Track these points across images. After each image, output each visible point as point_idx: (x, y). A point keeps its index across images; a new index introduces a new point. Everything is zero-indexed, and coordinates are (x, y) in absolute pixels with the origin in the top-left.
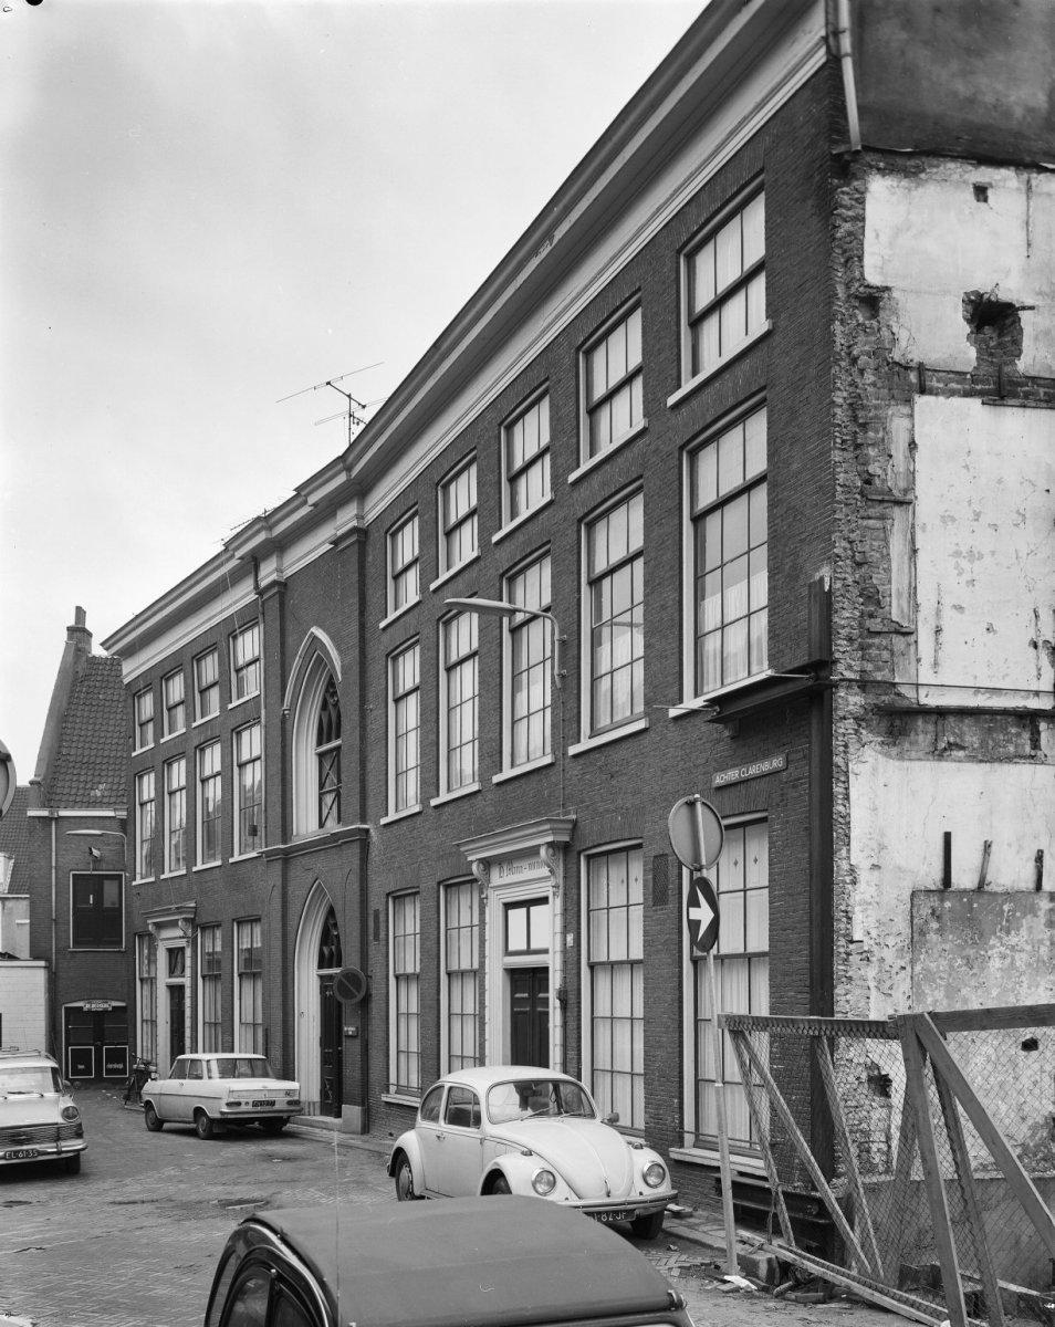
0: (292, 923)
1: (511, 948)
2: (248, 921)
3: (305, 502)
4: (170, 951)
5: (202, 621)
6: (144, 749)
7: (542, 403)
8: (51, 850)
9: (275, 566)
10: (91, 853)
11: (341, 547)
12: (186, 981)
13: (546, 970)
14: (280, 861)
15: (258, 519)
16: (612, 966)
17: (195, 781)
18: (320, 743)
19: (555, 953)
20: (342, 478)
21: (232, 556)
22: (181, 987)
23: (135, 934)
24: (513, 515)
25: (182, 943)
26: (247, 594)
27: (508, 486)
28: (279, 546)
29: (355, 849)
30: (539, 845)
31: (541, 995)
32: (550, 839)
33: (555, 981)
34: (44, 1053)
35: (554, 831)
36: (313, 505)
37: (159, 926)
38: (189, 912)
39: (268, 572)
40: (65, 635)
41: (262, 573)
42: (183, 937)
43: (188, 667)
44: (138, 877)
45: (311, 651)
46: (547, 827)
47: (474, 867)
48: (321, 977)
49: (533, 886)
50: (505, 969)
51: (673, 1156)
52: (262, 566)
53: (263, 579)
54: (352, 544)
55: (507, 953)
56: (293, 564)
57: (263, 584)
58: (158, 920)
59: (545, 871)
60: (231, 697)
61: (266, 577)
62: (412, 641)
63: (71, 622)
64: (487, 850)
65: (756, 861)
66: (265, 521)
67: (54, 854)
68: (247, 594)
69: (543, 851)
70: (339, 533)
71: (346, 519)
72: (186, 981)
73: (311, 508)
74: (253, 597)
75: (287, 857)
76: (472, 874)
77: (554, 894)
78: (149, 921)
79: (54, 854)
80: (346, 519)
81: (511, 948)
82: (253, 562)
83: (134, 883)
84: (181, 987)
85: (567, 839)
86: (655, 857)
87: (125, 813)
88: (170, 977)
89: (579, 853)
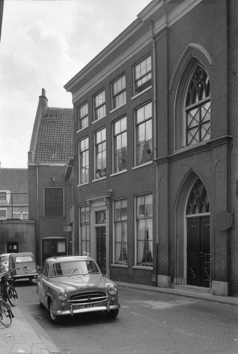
2: (119, 200)
4: (97, 213)
5: (113, 66)
7: (123, 78)
8: (36, 179)
9: (165, 21)
10: (52, 179)
12: (107, 225)
13: (105, 227)
17: (93, 148)
19: (107, 223)
22: (103, 229)
24: (114, 107)
25: (105, 208)
27: (113, 99)
30: (104, 198)
31: (104, 234)
32: (107, 196)
33: (107, 230)
34: (87, 264)
35: (107, 194)
40: (38, 99)
41: (156, 27)
42: (106, 205)
46: (106, 193)
47: (88, 203)
50: (95, 227)
51: (133, 268)
52: (156, 24)
59: (105, 204)
63: (41, 94)
67: (37, 180)
69: (104, 199)
72: (107, 225)
76: (87, 205)
77: (107, 209)
78: (87, 200)
79: (37, 180)
83: (78, 186)
84: (103, 229)
85: (110, 196)
87: (73, 157)
88: (97, 223)
89: (112, 200)
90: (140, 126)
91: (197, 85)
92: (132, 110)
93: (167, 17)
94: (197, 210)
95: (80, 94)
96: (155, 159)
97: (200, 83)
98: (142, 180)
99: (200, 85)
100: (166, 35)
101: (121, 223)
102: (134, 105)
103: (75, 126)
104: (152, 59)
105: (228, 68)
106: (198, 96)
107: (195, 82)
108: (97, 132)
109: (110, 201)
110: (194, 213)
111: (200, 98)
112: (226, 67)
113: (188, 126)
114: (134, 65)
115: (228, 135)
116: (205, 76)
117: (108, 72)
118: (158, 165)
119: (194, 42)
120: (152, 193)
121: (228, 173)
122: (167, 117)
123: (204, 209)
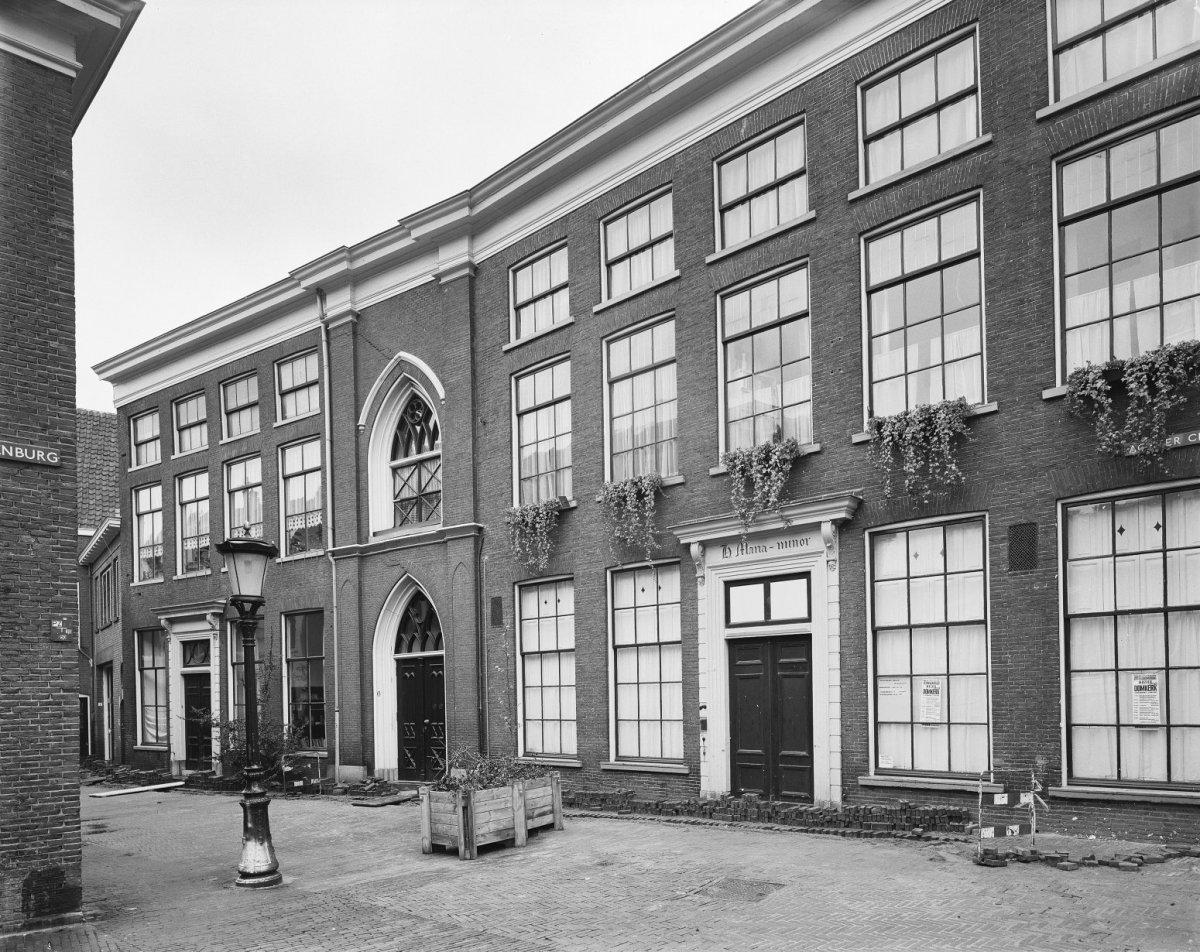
0: (369, 613)
1: (805, 615)
3: (409, 234)
6: (139, 468)
11: (443, 280)
14: (472, 540)
15: (342, 249)
16: (541, 654)
18: (394, 457)
20: (464, 213)
21: (298, 285)
23: (134, 630)
26: (314, 320)
28: (355, 279)
29: (470, 544)
36: (415, 239)
37: (172, 621)
38: (219, 608)
39: (339, 304)
43: (213, 395)
44: (136, 579)
45: (396, 374)
48: (398, 660)
49: (749, 568)
53: (329, 310)
54: (347, 323)
55: (728, 624)
56: (367, 298)
57: (330, 315)
58: (173, 616)
60: (276, 417)
61: (333, 308)
62: (563, 356)
64: (815, 516)
65: (643, 590)
66: (350, 253)
68: (314, 320)
70: (442, 268)
71: (454, 256)
73: (414, 241)
74: (318, 324)
75: (364, 555)
80: (454, 256)
81: (734, 620)
82: (320, 292)
86: (1010, 527)
90: (188, 505)
91: (413, 426)
92: (172, 476)
93: (471, 247)
94: (417, 645)
95: (283, 333)
96: (331, 548)
97: (419, 424)
98: (300, 584)
99: (418, 428)
100: (467, 279)
101: (1160, 617)
102: (279, 438)
103: (124, 455)
104: (321, 360)
105: (474, 411)
106: (429, 438)
107: (409, 420)
108: (184, 477)
109: (221, 622)
110: (410, 650)
111: (419, 451)
112: (470, 409)
113: (423, 487)
114: (280, 362)
115: (475, 521)
116: (428, 414)
117: (206, 364)
118: (335, 560)
119: (408, 351)
120: (572, 579)
121: (476, 585)
122: (354, 474)
123: (430, 643)
